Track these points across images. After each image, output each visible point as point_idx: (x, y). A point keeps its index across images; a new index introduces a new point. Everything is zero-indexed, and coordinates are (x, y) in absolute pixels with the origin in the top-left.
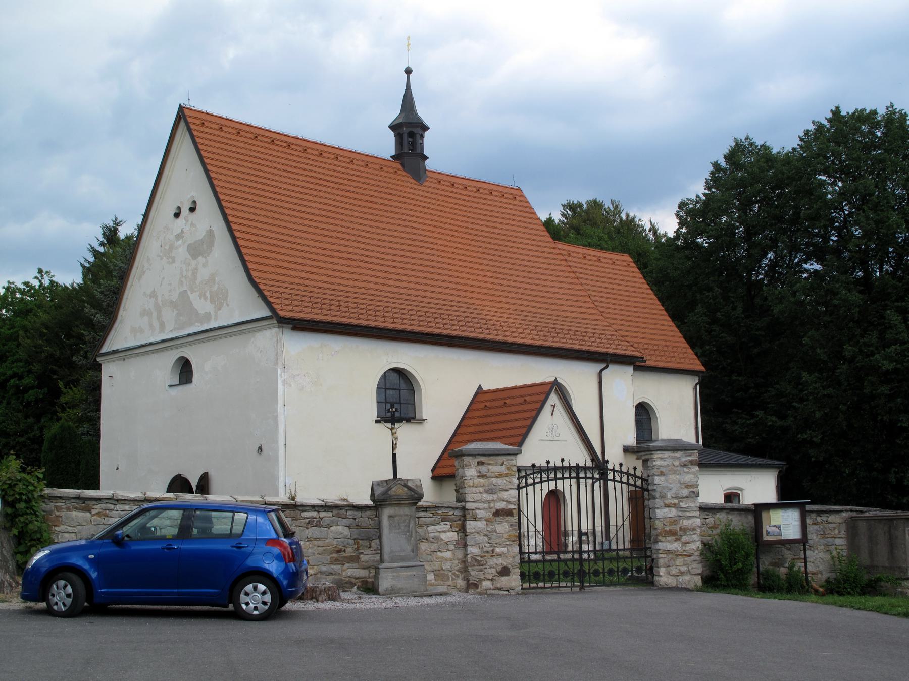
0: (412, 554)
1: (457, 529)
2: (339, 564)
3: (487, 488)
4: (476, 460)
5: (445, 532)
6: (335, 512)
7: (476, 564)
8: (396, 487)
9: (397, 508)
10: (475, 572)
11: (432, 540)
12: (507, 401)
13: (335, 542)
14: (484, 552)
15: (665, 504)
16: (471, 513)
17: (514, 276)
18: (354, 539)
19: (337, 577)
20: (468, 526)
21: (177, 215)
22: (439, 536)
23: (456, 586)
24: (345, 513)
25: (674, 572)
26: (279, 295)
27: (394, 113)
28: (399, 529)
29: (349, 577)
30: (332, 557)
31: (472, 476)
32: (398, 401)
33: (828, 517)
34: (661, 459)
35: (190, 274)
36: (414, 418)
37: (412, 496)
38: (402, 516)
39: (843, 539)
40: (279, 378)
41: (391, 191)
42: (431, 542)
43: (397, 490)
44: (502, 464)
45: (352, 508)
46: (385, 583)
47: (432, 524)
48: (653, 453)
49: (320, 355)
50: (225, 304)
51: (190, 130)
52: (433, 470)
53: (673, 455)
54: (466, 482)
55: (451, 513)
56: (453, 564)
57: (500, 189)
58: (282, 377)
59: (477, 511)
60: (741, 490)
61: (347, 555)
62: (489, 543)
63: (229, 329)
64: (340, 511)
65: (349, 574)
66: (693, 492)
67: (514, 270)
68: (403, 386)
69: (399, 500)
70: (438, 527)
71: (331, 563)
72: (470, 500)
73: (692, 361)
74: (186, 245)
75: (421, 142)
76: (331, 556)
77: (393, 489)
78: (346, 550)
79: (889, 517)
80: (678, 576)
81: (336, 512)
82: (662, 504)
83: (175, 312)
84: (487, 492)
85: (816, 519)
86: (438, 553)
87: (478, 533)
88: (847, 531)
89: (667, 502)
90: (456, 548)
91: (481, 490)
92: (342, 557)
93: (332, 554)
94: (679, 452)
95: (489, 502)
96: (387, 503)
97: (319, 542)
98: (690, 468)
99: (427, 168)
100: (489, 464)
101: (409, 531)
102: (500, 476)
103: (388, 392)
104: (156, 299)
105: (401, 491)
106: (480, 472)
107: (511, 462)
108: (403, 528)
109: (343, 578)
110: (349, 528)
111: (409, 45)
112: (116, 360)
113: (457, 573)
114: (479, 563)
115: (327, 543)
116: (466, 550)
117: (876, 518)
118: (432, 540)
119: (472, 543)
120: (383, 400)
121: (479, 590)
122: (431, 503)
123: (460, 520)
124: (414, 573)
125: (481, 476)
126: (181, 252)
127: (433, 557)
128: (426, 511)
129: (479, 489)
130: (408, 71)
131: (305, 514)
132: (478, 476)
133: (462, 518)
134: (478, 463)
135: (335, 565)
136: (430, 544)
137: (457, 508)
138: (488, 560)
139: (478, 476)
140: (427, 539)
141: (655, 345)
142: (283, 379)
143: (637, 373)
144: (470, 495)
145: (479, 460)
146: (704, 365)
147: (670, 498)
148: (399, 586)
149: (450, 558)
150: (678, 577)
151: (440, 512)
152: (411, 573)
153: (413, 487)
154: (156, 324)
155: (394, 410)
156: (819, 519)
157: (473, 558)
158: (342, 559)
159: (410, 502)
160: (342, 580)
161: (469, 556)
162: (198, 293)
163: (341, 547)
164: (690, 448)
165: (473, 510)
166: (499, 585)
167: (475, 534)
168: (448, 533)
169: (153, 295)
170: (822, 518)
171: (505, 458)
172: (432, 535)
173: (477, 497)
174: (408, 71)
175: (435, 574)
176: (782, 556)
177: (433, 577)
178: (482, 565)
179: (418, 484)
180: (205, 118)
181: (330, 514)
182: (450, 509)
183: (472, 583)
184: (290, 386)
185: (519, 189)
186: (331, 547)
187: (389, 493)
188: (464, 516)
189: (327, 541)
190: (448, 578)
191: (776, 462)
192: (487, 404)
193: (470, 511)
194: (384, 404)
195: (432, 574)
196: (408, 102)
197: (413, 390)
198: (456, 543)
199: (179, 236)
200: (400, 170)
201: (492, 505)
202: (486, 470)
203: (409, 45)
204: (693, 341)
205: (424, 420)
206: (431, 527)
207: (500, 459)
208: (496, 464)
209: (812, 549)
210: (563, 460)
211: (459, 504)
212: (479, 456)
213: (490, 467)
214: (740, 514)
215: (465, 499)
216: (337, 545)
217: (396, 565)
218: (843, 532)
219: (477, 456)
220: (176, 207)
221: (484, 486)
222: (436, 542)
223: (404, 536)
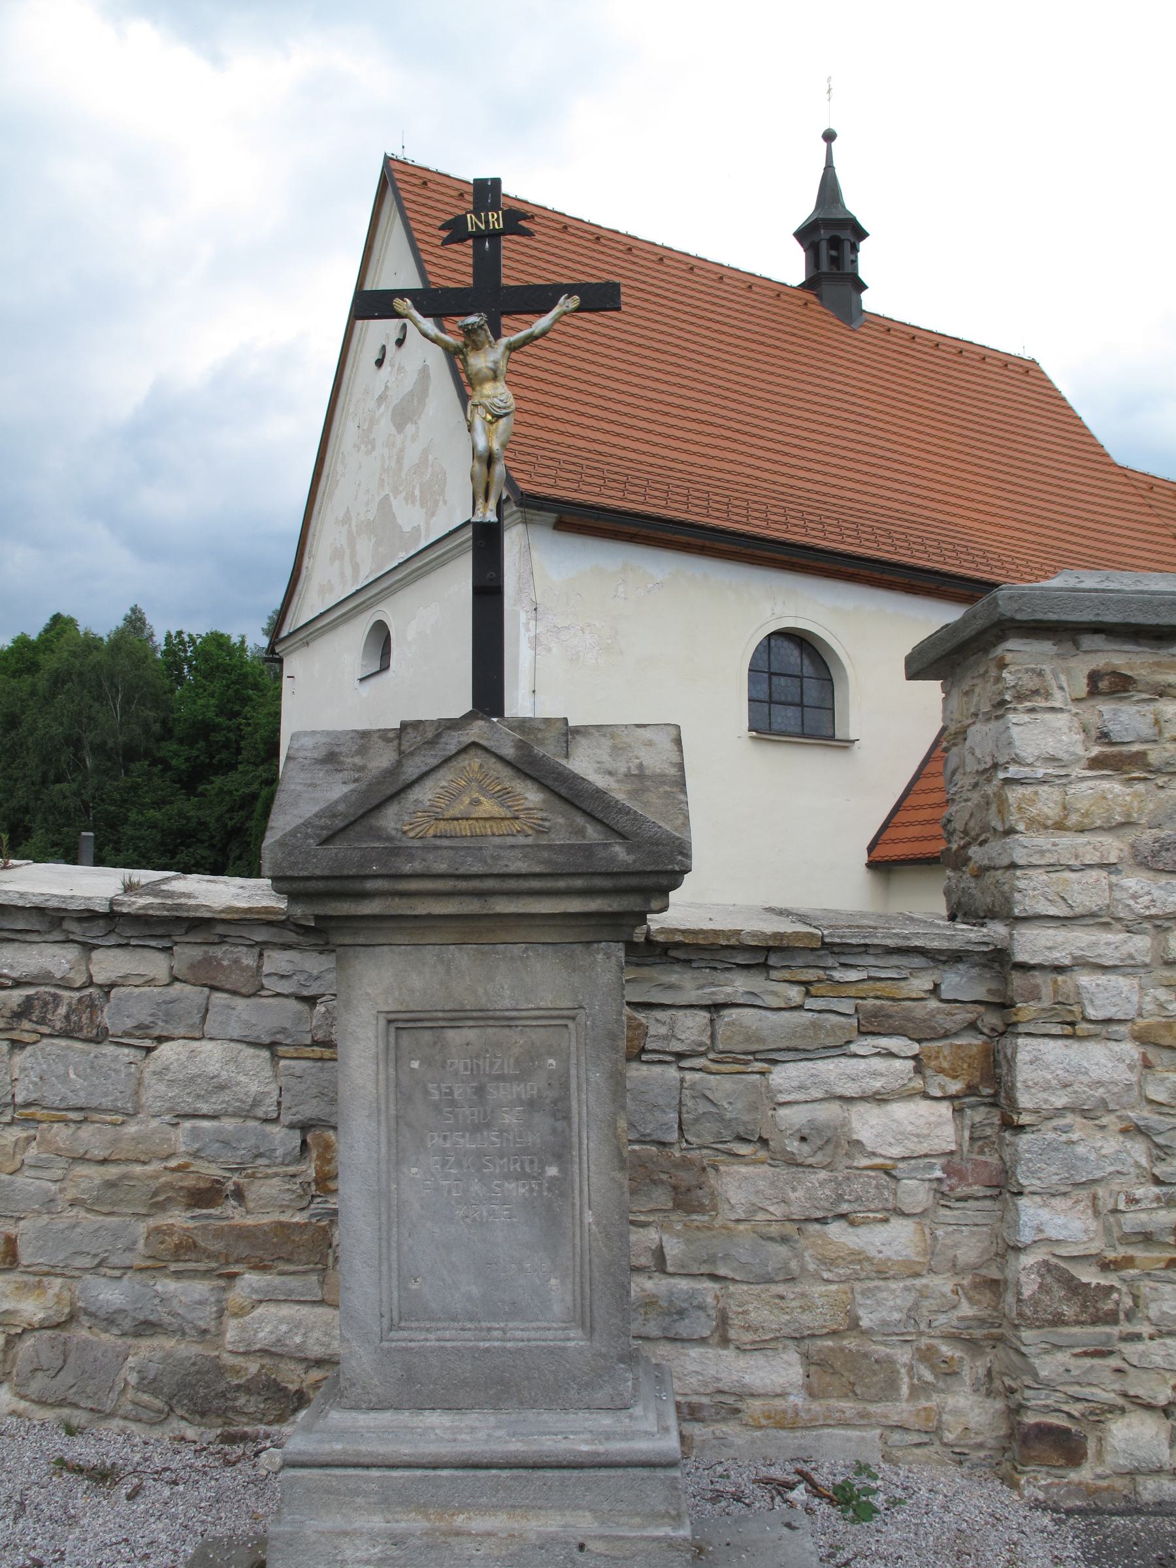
0: (576, 1340)
1: (955, 1087)
2: (206, 1274)
3: (1148, 836)
5: (879, 1098)
6: (188, 953)
7: (1068, 1311)
8: (444, 779)
9: (462, 957)
10: (1062, 1357)
11: (794, 1146)
13: (181, 1138)
14: (1126, 1239)
16: (1046, 992)
18: (305, 1127)
19: (187, 1350)
20: (1024, 1073)
22: (845, 1123)
23: (938, 1431)
24: (248, 960)
27: (804, 208)
28: (476, 1128)
29: (264, 1352)
30: (157, 1230)
31: (1052, 759)
32: (797, 700)
35: (393, 463)
36: (832, 737)
37: (587, 850)
38: (507, 1021)
40: (522, 631)
42: (793, 1162)
43: (454, 797)
45: (291, 937)
49: (621, 589)
50: (441, 503)
51: (402, 210)
52: (871, 849)
54: (1014, 795)
55: (921, 984)
58: (528, 630)
59: (1085, 980)
61: (250, 1221)
62: (1157, 1181)
64: (218, 952)
65: (264, 1337)
67: (1032, 480)
68: (808, 670)
70: (831, 1069)
71: (155, 1267)
74: (390, 410)
75: (852, 257)
76: (152, 1222)
77: (425, 794)
78: (250, 1195)
81: (197, 953)
83: (373, 540)
86: (835, 1229)
87: (1085, 1113)
90: (942, 1195)
91: (1113, 847)
92: (219, 1234)
93: (161, 1207)
97: (86, 1131)
101: (561, 1152)
103: (775, 679)
104: (350, 526)
105: (488, 807)
106: (1104, 737)
108: (510, 1118)
109: (228, 1359)
110: (275, 1057)
112: (297, 648)
113: (946, 1350)
115: (137, 1140)
118: (794, 1146)
119: (1053, 1174)
120: (763, 696)
121: (1085, 1474)
122: (802, 918)
123: (972, 1026)
124: (585, 1524)
126: (385, 426)
127: (799, 1256)
128: (765, 967)
129: (1096, 839)
130: (829, 137)
132: (1096, 763)
133: (992, 1019)
135: (178, 1275)
136: (784, 1172)
137: (956, 957)
138: (1146, 1287)
139: (1096, 763)
140: (764, 1142)
142: (532, 634)
144: (1040, 877)
145: (1098, 662)
149: (908, 1263)
151: (853, 975)
152: (550, 1523)
153: (600, 781)
154: (348, 571)
158: (217, 1246)
159: (574, 905)
160: (220, 1370)
162: (403, 494)
163: (215, 1171)
165: (1059, 969)
167: (1069, 1119)
168: (901, 1111)
169: (347, 520)
174: (829, 137)
175: (806, 1356)
178: (1111, 1318)
179: (656, 760)
180: (426, 179)
181: (155, 965)
182: (918, 961)
184: (549, 650)
186: (156, 1166)
187: (390, 820)
188: (1004, 1006)
189: (132, 1129)
190: (892, 1385)
193: (1038, 978)
195: (793, 1357)
196: (829, 189)
197: (831, 680)
198: (947, 1169)
199: (382, 399)
200: (814, 303)
202: (1145, 728)
205: (853, 741)
211: (966, 934)
212: (1098, 641)
215: (1008, 901)
216: (196, 1155)
219: (1087, 641)
220: (379, 347)
221: (1127, 824)
222: (818, 1158)
223: (517, 1190)
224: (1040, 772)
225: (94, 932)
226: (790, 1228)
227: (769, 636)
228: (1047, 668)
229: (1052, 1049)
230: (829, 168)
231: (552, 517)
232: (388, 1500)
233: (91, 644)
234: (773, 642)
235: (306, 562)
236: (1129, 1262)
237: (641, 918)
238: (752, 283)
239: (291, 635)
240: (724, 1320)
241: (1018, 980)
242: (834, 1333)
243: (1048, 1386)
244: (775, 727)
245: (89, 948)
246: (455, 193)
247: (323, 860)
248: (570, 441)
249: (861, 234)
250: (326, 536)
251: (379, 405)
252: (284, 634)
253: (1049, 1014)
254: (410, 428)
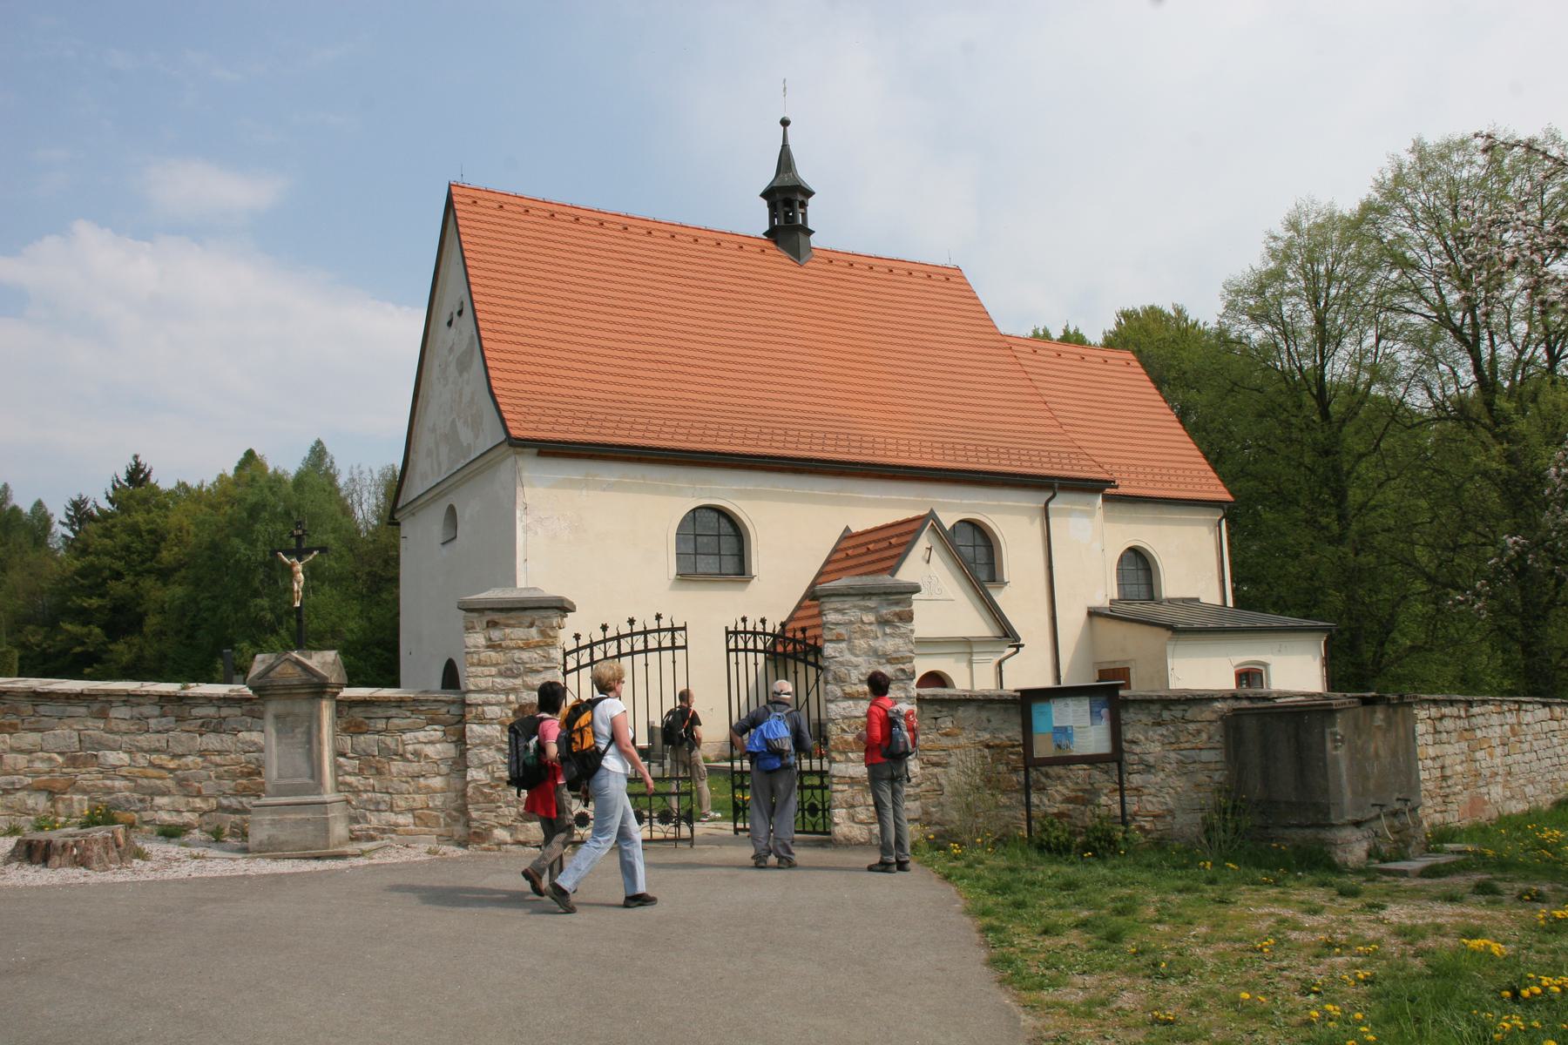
0: (311, 781)
1: (454, 739)
4: (485, 620)
5: (432, 743)
7: (481, 799)
12: (871, 546)
15: (845, 694)
16: (474, 711)
17: (1098, 414)
21: (450, 324)
25: (862, 817)
26: (571, 414)
27: (766, 175)
33: (1185, 710)
34: (837, 610)
39: (1218, 752)
41: (751, 275)
44: (531, 625)
46: (258, 835)
47: (411, 730)
48: (822, 600)
53: (862, 603)
55: (444, 710)
56: (446, 797)
57: (941, 271)
60: (1265, 665)
63: (477, 462)
66: (903, 671)
69: (285, 687)
70: (421, 735)
72: (472, 688)
73: (1213, 488)
77: (278, 669)
79: (1295, 709)
80: (872, 823)
81: (248, 708)
82: (839, 693)
84: (500, 674)
85: (1160, 715)
86: (421, 779)
88: (1226, 736)
89: (848, 690)
91: (494, 670)
92: (255, 784)
94: (874, 598)
95: (507, 692)
96: (268, 692)
98: (898, 627)
99: (812, 245)
100: (508, 626)
102: (528, 646)
106: (490, 639)
107: (547, 621)
108: (299, 736)
111: (785, 89)
113: (454, 813)
114: (488, 799)
116: (465, 776)
117: (1274, 711)
124: (309, 816)
125: (492, 646)
126: (452, 369)
128: (400, 707)
130: (785, 123)
131: (197, 712)
134: (488, 623)
135: (244, 796)
139: (488, 647)
140: (401, 755)
141: (1179, 469)
143: (1109, 506)
146: (1231, 493)
147: (857, 681)
148: (282, 838)
150: (872, 826)
152: (303, 816)
155: (300, 532)
156: (1166, 715)
157: (478, 789)
159: (307, 691)
161: (470, 786)
164: (894, 590)
166: (521, 838)
168: (438, 745)
170: (1173, 713)
171: (536, 615)
172: (410, 748)
173: (483, 683)
174: (785, 123)
175: (414, 817)
176: (1092, 784)
177: (412, 820)
178: (492, 801)
181: (238, 711)
183: (475, 833)
184: (536, 533)
185: (958, 269)
187: (272, 674)
188: (463, 716)
191: (1320, 624)
192: (850, 552)
194: (693, 557)
196: (785, 161)
200: (771, 248)
201: (512, 697)
203: (785, 89)
204: (1216, 458)
206: (408, 734)
207: (527, 617)
208: (520, 625)
209: (1153, 771)
210: (658, 617)
213: (508, 631)
214: (1006, 710)
217: (283, 800)
218: (1217, 738)
219: (487, 612)
224: (472, 650)
225: (220, 703)
226: (409, 779)
227: (694, 510)
228: (475, 621)
229: (475, 727)
230: (785, 146)
231: (535, 451)
232: (272, 813)
233: (277, 480)
234: (697, 514)
235: (412, 456)
236: (498, 786)
237: (338, 693)
238: (719, 239)
239: (403, 507)
240: (392, 805)
241: (467, 709)
242: (422, 809)
243: (475, 820)
244: (700, 570)
245: (219, 707)
246: (496, 205)
247: (258, 683)
248: (556, 390)
249: (809, 193)
250: (424, 441)
251: (450, 354)
252: (399, 506)
253: (475, 717)
254: (465, 375)
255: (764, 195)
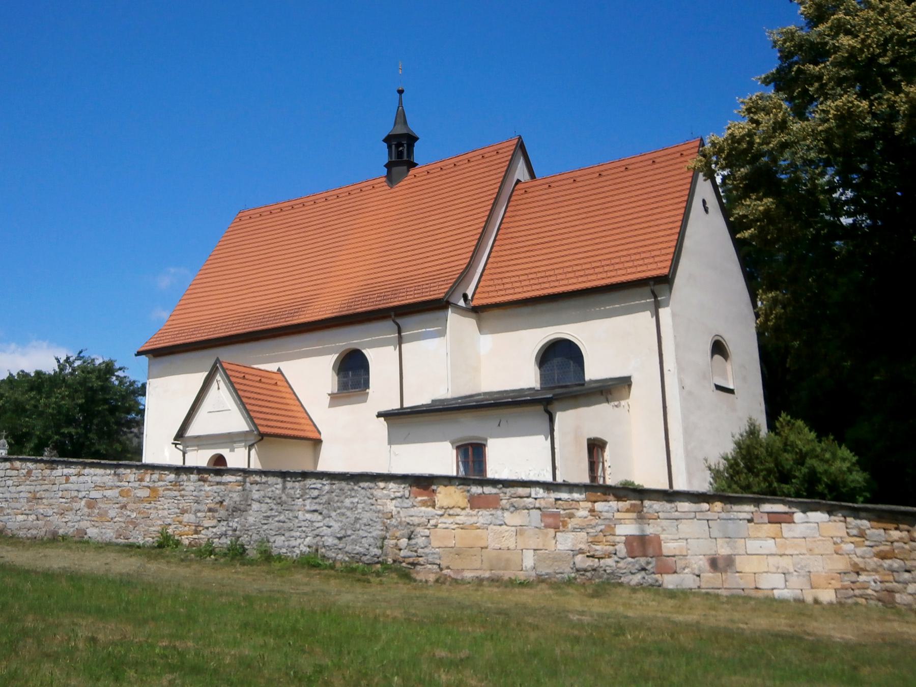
130: (401, 92)
174: (401, 92)
196: (401, 117)
255: (385, 140)
